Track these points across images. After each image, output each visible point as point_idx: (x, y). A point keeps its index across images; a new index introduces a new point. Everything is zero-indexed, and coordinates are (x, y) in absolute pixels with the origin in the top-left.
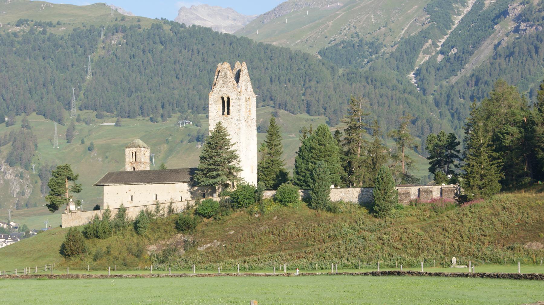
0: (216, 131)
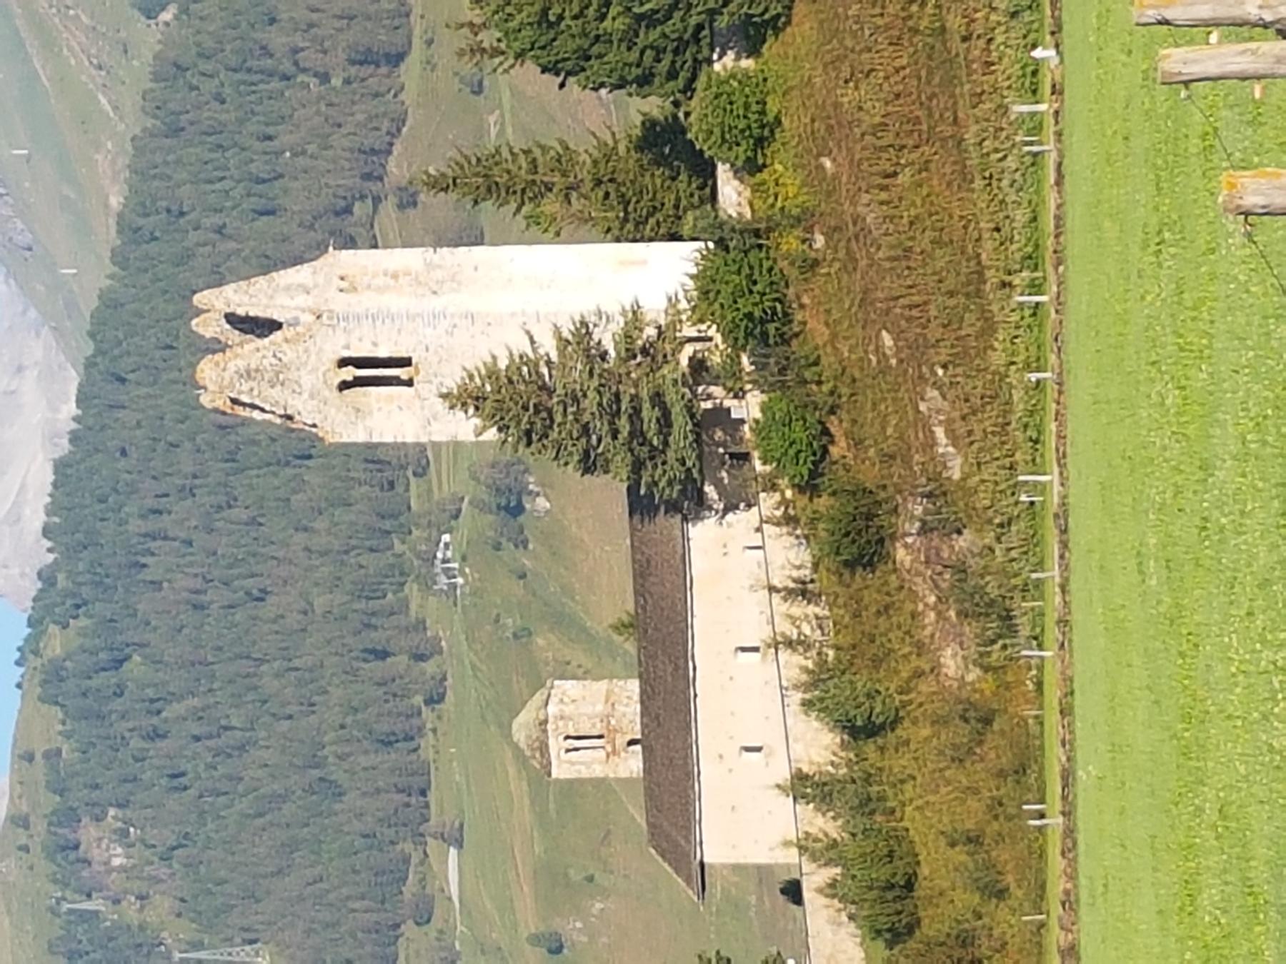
0: (477, 408)
